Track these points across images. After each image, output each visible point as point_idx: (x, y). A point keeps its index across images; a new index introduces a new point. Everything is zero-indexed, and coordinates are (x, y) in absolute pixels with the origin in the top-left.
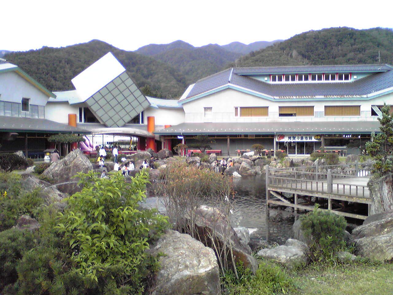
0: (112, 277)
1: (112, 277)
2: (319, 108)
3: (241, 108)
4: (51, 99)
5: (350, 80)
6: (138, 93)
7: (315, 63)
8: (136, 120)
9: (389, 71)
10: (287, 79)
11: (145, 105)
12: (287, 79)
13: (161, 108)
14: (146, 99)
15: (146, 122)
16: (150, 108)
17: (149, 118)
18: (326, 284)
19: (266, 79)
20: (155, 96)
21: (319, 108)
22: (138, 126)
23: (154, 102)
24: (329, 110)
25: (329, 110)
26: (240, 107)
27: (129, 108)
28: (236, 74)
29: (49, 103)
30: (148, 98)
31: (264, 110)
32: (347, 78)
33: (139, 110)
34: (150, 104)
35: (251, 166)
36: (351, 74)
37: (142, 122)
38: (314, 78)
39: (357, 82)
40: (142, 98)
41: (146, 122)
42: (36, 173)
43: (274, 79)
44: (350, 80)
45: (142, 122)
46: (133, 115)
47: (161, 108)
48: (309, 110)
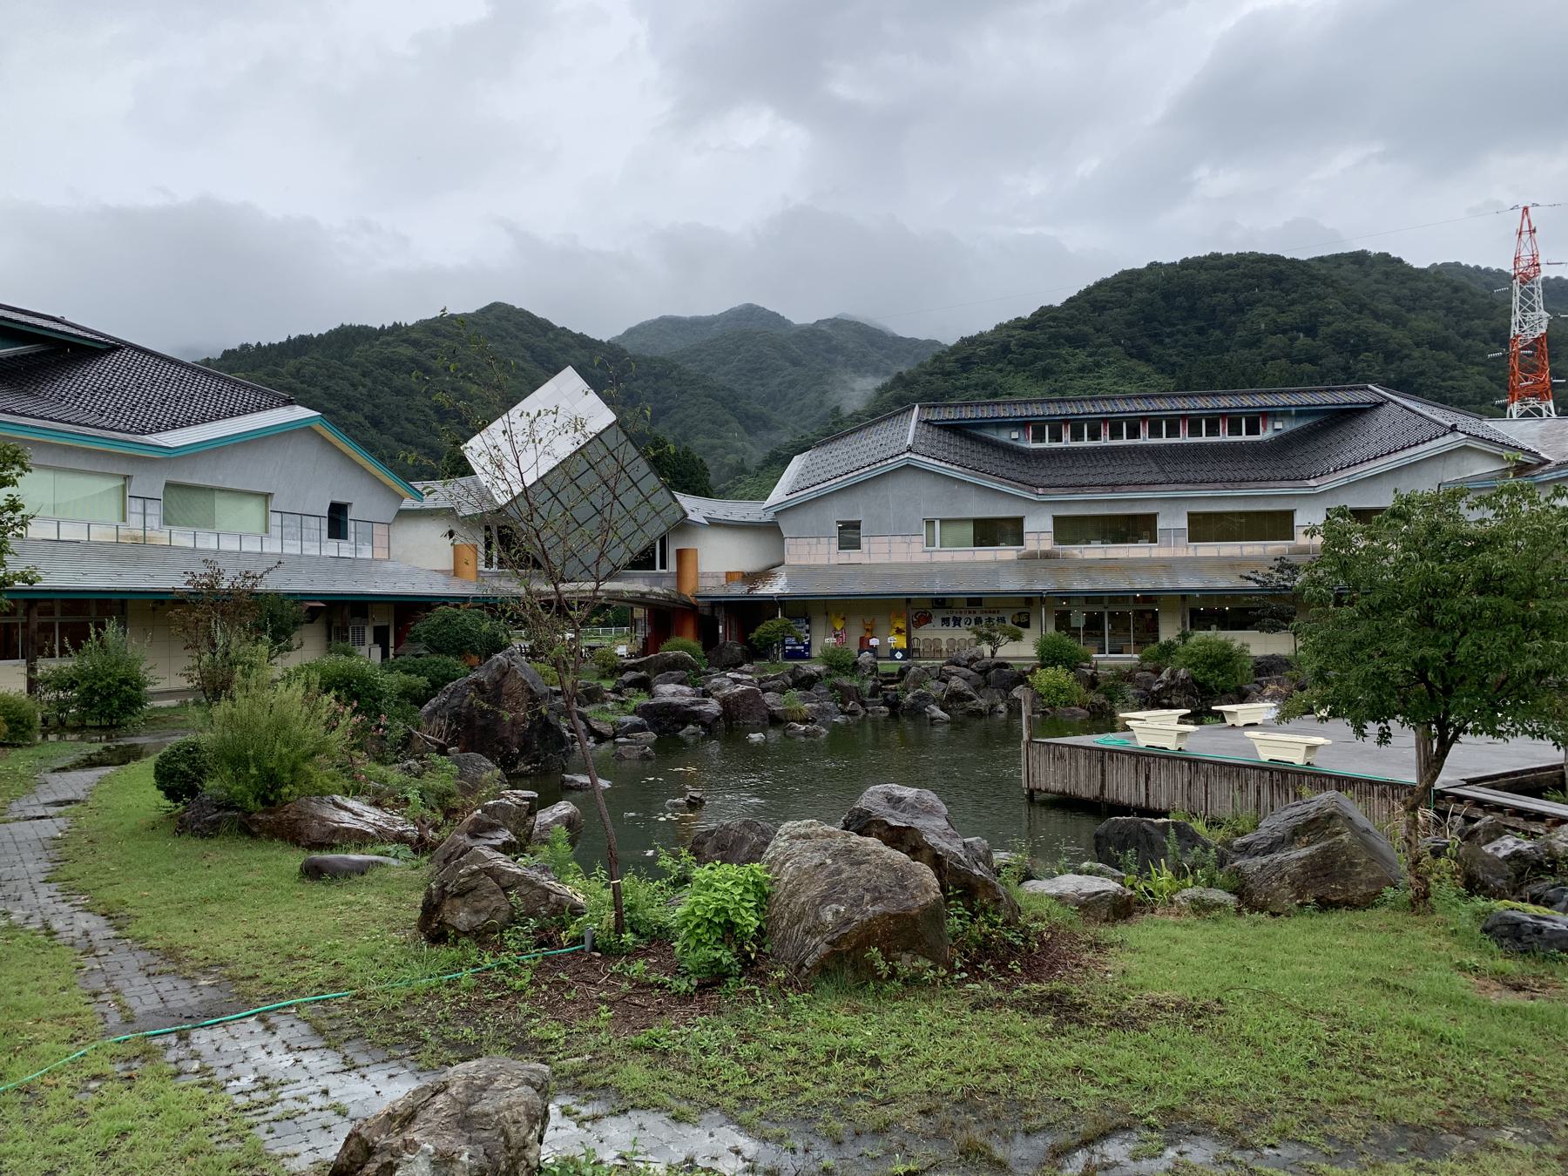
0: (678, 950)
1: (678, 950)
2: (1173, 521)
3: (942, 521)
4: (408, 503)
5: (1266, 434)
6: (652, 481)
7: (1186, 387)
8: (644, 561)
9: (1381, 404)
10: (1116, 434)
11: (672, 516)
12: (1116, 434)
13: (715, 524)
14: (675, 500)
15: (672, 565)
16: (683, 525)
17: (680, 553)
18: (774, 1126)
19: (1015, 435)
20: (704, 491)
21: (1173, 521)
22: (649, 576)
23: (695, 507)
24: (1203, 527)
25: (1068, 529)
26: (942, 521)
27: (627, 528)
28: (927, 422)
29: (404, 514)
30: (679, 496)
31: (1068, 529)
32: (1252, 430)
33: (655, 529)
34: (686, 515)
35: (976, 688)
36: (1265, 415)
37: (663, 566)
38: (1155, 432)
39: (1283, 444)
40: (662, 498)
41: (672, 565)
42: (58, 726)
43: (1039, 437)
44: (1266, 434)
45: (663, 566)
46: (638, 544)
47: (715, 524)
48: (1139, 528)
